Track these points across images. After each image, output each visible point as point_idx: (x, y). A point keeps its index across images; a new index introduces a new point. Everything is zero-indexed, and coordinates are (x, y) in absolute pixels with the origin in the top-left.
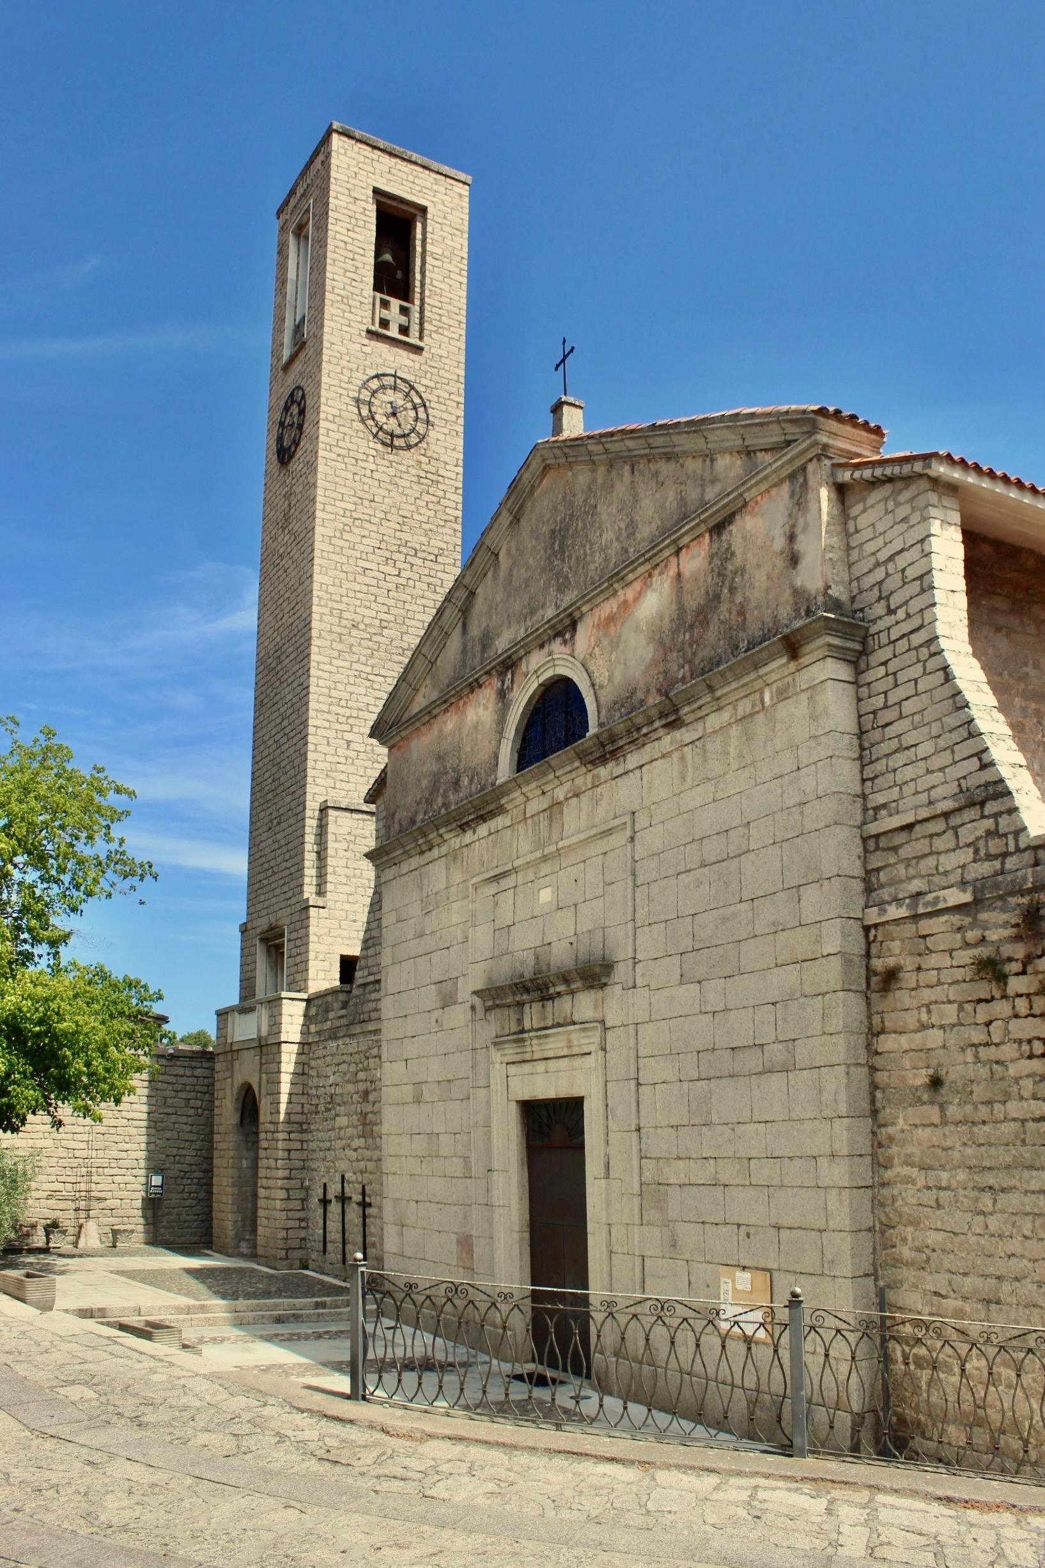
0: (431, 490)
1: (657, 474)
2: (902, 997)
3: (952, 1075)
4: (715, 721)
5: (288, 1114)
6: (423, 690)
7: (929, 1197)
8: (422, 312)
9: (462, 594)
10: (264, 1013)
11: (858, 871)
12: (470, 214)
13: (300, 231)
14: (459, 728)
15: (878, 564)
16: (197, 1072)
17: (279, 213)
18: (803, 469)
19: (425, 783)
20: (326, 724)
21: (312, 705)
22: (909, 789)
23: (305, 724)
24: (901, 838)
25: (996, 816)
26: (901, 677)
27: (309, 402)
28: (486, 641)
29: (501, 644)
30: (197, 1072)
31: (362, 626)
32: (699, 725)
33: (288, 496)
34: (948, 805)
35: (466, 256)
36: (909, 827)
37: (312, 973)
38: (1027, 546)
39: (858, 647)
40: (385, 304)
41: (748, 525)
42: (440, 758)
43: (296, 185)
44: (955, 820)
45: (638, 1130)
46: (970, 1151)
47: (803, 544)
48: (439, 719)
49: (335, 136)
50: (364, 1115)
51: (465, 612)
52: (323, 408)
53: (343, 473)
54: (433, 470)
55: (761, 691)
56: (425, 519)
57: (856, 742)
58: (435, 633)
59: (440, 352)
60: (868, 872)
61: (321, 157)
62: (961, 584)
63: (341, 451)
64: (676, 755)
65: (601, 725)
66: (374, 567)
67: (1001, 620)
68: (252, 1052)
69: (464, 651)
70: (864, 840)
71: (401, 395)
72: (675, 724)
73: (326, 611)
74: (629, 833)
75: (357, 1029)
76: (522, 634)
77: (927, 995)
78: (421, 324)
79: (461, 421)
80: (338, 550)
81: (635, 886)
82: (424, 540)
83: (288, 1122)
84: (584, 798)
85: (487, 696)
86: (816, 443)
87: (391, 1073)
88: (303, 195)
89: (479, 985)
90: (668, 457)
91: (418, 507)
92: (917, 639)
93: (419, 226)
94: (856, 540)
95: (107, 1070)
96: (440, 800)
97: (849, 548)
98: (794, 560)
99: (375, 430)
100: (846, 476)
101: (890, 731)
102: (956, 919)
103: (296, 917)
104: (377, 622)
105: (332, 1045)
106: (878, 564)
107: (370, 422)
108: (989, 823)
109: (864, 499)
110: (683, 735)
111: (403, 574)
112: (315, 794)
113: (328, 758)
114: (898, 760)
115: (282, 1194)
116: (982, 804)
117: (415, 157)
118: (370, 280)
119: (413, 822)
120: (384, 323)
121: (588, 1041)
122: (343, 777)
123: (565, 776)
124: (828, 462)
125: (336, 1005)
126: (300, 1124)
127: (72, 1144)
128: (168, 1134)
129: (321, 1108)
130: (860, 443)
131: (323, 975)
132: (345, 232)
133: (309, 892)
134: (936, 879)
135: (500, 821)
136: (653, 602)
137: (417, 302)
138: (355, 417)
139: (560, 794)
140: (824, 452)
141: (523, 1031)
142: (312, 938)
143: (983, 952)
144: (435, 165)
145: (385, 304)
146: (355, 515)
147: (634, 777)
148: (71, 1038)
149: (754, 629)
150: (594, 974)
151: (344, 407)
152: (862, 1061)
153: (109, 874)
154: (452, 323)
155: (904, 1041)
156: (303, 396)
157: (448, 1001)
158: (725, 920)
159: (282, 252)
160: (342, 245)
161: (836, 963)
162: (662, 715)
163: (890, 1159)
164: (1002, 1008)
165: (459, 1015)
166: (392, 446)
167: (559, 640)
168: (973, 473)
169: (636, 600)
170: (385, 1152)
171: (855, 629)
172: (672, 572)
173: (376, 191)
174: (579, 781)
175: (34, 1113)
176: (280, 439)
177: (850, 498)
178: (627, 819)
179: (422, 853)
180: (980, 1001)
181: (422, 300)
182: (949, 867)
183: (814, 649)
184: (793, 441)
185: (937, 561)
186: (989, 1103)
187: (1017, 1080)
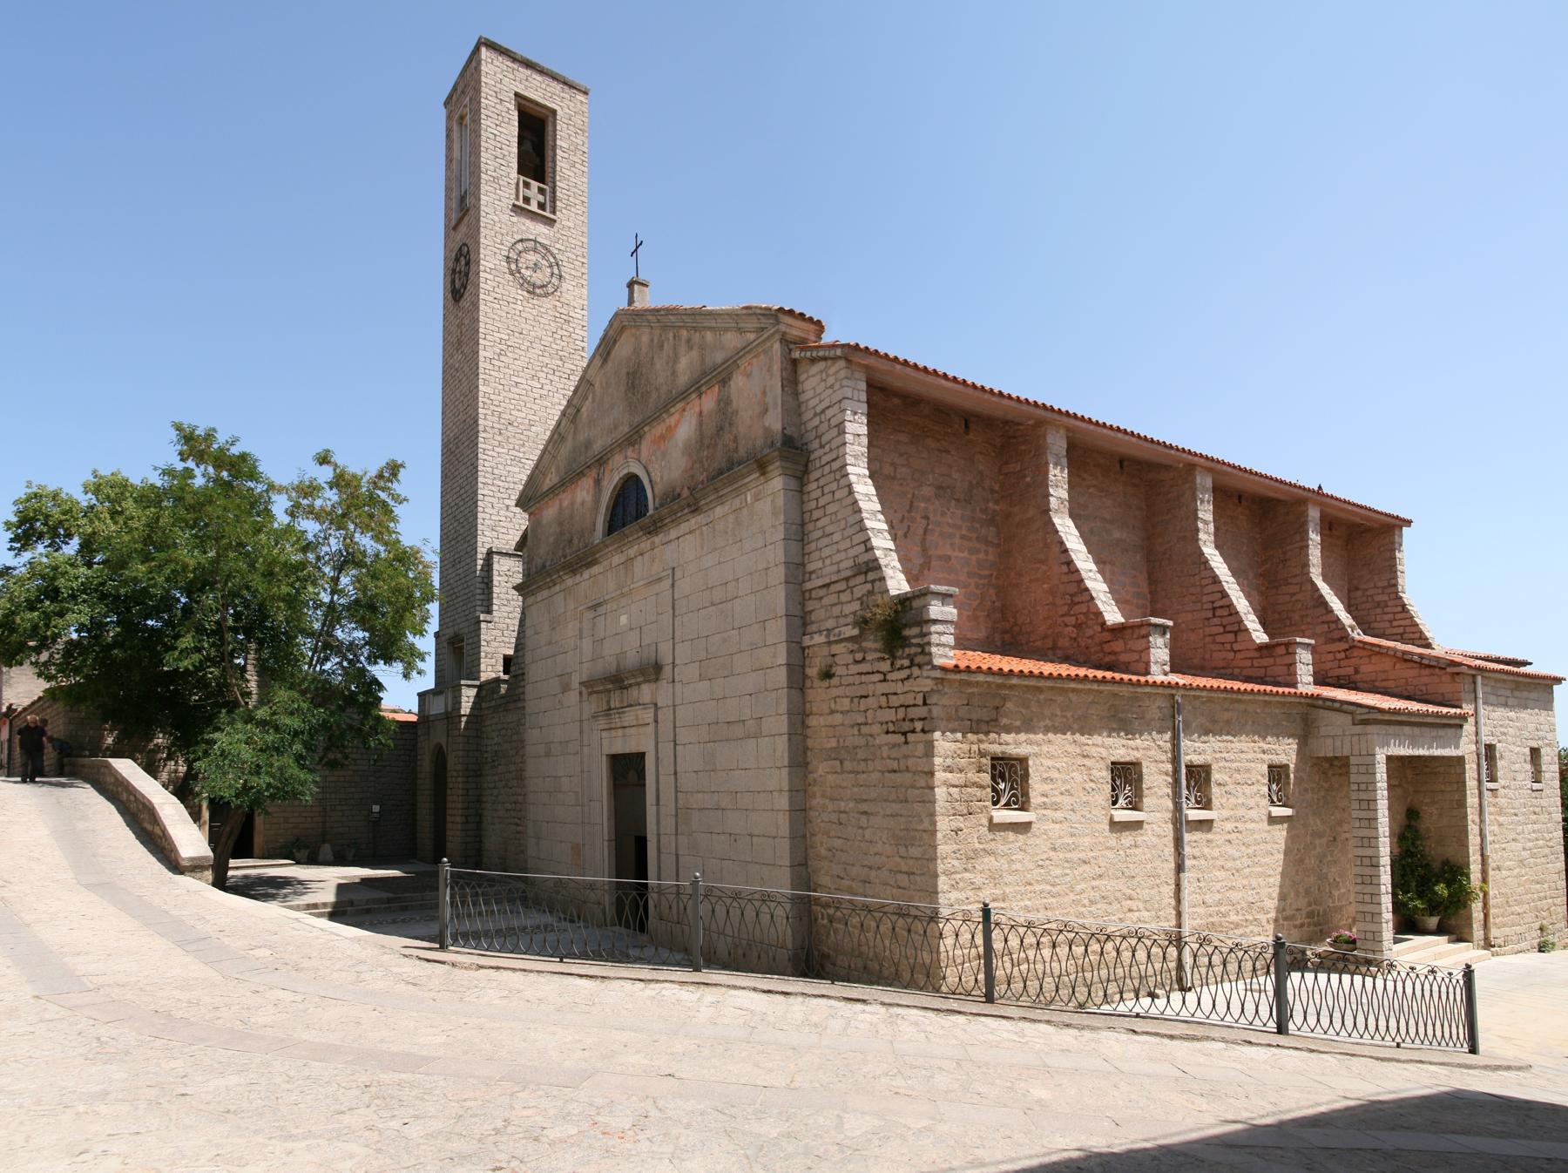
14: (572, 504)
15: (816, 415)
21: (480, 479)
22: (828, 562)
24: (822, 592)
25: (873, 582)
26: (826, 490)
34: (849, 573)
36: (827, 586)
37: (483, 667)
42: (561, 524)
44: (852, 583)
51: (574, 421)
75: (512, 706)
92: (836, 465)
101: (820, 524)
102: (850, 646)
106: (816, 415)
108: (869, 586)
112: (485, 541)
118: (515, 166)
119: (544, 567)
131: (490, 668)
135: (596, 569)
136: (684, 427)
147: (673, 545)
149: (742, 452)
150: (653, 670)
155: (822, 721)
161: (784, 670)
162: (689, 505)
165: (572, 697)
171: (800, 454)
173: (517, 94)
176: (453, 282)
182: (837, 615)
183: (775, 468)
187: (880, 747)
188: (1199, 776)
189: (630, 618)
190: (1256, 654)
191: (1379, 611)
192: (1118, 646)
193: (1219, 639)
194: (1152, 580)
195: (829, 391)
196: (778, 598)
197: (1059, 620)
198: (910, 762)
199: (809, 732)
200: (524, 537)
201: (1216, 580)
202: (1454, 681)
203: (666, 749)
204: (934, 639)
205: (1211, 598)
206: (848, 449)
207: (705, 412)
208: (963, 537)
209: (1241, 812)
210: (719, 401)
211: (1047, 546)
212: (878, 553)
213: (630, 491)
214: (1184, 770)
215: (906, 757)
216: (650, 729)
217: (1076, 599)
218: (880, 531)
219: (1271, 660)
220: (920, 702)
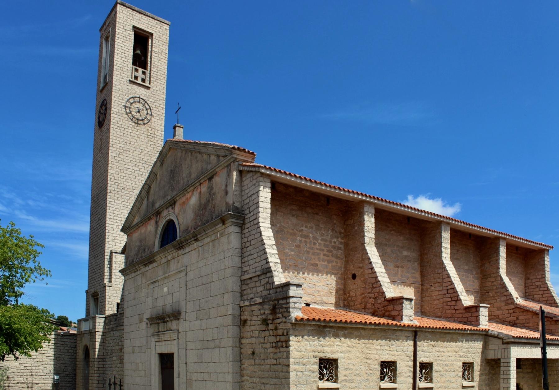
0: (152, 140)
1: (197, 157)
2: (247, 328)
3: (257, 351)
4: (207, 240)
5: (98, 355)
6: (137, 217)
7: (251, 385)
8: (150, 74)
9: (147, 187)
10: (91, 322)
11: (238, 290)
12: (169, 37)
13: (107, 39)
16: (72, 341)
17: (100, 30)
18: (230, 164)
19: (136, 249)
20: (113, 223)
21: (108, 216)
23: (105, 223)
24: (249, 281)
25: (269, 277)
27: (108, 106)
28: (153, 204)
29: (157, 205)
30: (72, 341)
31: (126, 189)
32: (203, 241)
33: (101, 139)
34: (258, 273)
35: (167, 52)
36: (251, 278)
37: (107, 309)
38: (306, 188)
39: (242, 222)
40: (137, 70)
41: (217, 179)
42: (141, 241)
43: (106, 21)
44: (261, 278)
45: (186, 363)
46: (260, 373)
47: (229, 189)
48: (141, 228)
49: (118, 5)
50: (121, 356)
51: (148, 192)
52: (112, 109)
53: (120, 133)
54: (153, 133)
55: (217, 233)
56: (149, 150)
57: (240, 251)
58: (139, 199)
59: (157, 89)
60: (242, 291)
61: (114, 13)
62: (269, 206)
63: (119, 125)
64: (197, 249)
65: (180, 237)
67: (294, 213)
68: (88, 335)
69: (147, 206)
70: (241, 281)
71: (141, 105)
72: (197, 240)
73: (113, 183)
74: (185, 273)
75: (119, 328)
76: (162, 203)
77: (253, 328)
78: (150, 78)
79: (164, 115)
80: (117, 161)
81: (187, 289)
82: (149, 158)
83: (98, 358)
84: (176, 259)
85: (152, 222)
86: (233, 157)
87: (127, 343)
88: (108, 25)
89: (149, 316)
90: (200, 153)
91: (147, 146)
92: (255, 222)
93: (150, 40)
94: (244, 188)
95: (33, 340)
96: (140, 255)
97: (242, 191)
98: (227, 193)
99: (131, 118)
100: (241, 168)
102: (259, 306)
103: (102, 289)
104: (131, 187)
105: (112, 333)
106: (248, 197)
107: (130, 115)
108: (267, 280)
109: (246, 176)
110: (199, 244)
111: (141, 170)
113: (113, 235)
115: (97, 382)
116: (266, 274)
117: (149, 14)
118: (131, 61)
119: (133, 261)
120: (136, 78)
121: (174, 336)
122: (119, 241)
123: (171, 253)
124: (237, 163)
125: (113, 320)
126: (102, 358)
127: (26, 365)
128: (62, 362)
129: (109, 354)
130: (248, 157)
132: (121, 42)
133: (106, 281)
134: (256, 294)
135: (155, 264)
136: (194, 200)
137: (149, 70)
138: (124, 113)
139: (170, 258)
140: (236, 160)
141: (159, 332)
142: (107, 297)
143: (264, 317)
144: (157, 17)
145: (137, 70)
146: (124, 149)
147: (187, 255)
148: (19, 331)
151: (120, 109)
152: (238, 346)
153: (35, 273)
154: (161, 78)
156: (106, 103)
157: (141, 321)
158: (207, 302)
159: (101, 46)
160: (120, 47)
161: (231, 317)
162: (193, 237)
163: (244, 374)
164: (267, 333)
165: (143, 325)
166: (138, 123)
167: (171, 208)
168: (274, 171)
169: (190, 198)
170: (125, 368)
171: (243, 217)
172: (199, 191)
173: (134, 27)
174: (174, 254)
175: (8, 355)
176: (99, 118)
177: (243, 175)
178: (185, 268)
179: (135, 272)
180: (263, 331)
181: (150, 69)
182: (257, 292)
183: (229, 222)
184: (228, 155)
185: (261, 199)
186: (264, 359)
187: (270, 353)
188: (426, 368)
189: (168, 289)
190: (464, 312)
191: (537, 289)
192: (390, 307)
193: (449, 304)
194: (422, 275)
195: (254, 187)
197: (367, 295)
198: (281, 360)
200: (125, 246)
201: (448, 276)
202: (556, 324)
204: (292, 305)
205: (446, 285)
206: (260, 214)
207: (202, 192)
208: (324, 255)
209: (447, 384)
210: (208, 188)
211: (363, 260)
212: (271, 265)
213: (170, 227)
214: (418, 365)
215: (280, 358)
217: (374, 286)
218: (273, 254)
219: (470, 314)
220: (285, 334)
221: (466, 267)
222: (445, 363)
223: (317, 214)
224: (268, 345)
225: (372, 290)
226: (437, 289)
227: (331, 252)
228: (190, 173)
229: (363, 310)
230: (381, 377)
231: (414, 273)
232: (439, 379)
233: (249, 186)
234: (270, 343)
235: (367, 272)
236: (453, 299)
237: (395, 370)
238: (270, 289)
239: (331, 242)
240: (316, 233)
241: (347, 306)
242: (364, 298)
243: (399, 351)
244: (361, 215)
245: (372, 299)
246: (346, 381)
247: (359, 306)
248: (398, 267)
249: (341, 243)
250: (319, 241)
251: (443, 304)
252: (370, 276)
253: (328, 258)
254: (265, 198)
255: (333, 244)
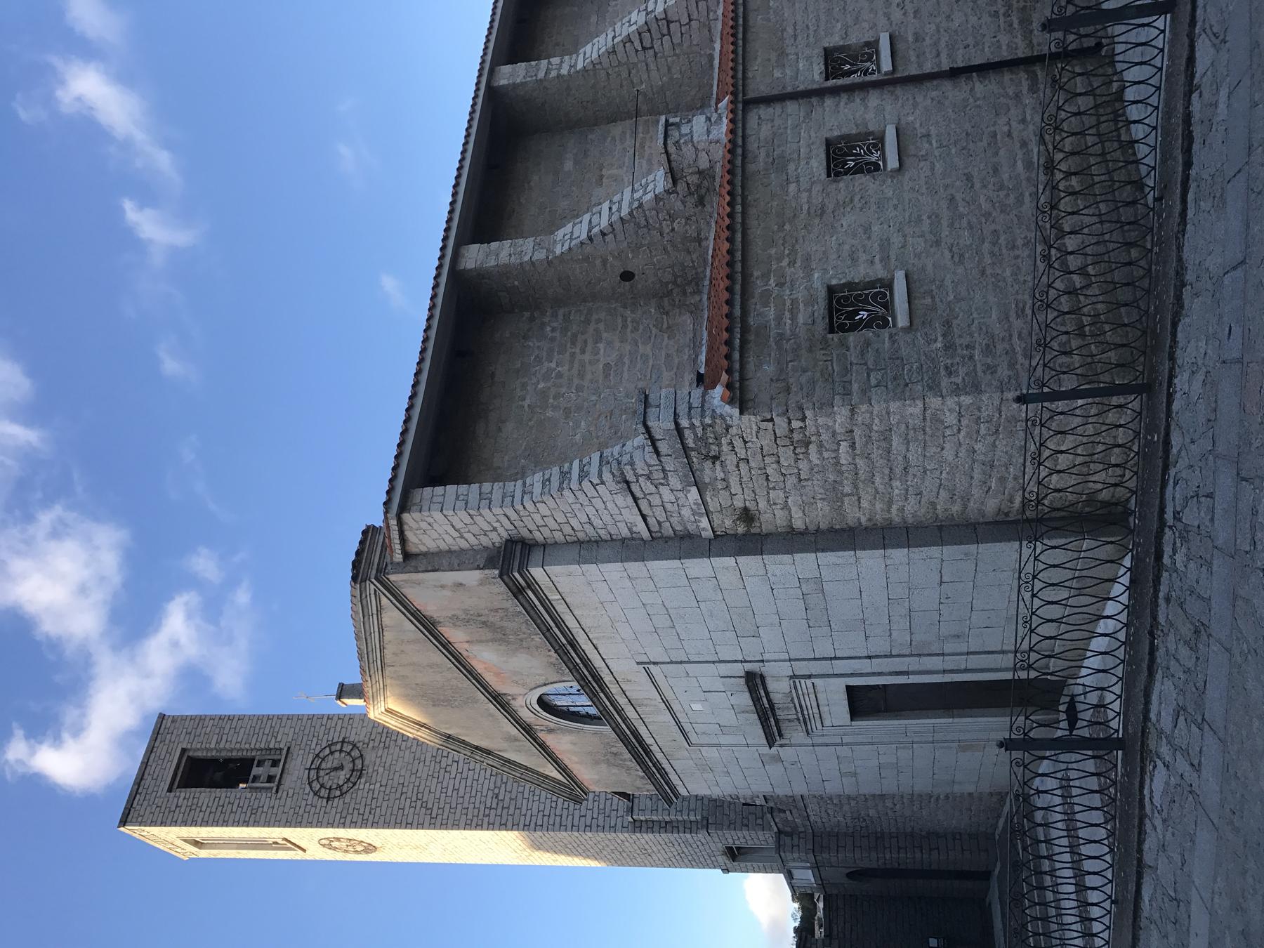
7: (912, 500)
15: (462, 537)
19: (615, 771)
22: (619, 518)
24: (651, 521)
31: (496, 791)
36: (644, 517)
39: (519, 547)
42: (597, 763)
44: (639, 494)
46: (878, 480)
66: (452, 781)
73: (486, 819)
101: (577, 526)
106: (462, 537)
107: (345, 788)
114: (597, 522)
125: (782, 815)
146: (414, 799)
150: (754, 682)
157: (778, 759)
165: (786, 753)
172: (466, 646)
193: (677, 40)
194: (613, 119)
195: (435, 526)
196: (663, 568)
199: (812, 528)
203: (840, 667)
207: (468, 638)
208: (583, 352)
214: (831, 83)
216: (817, 681)
217: (643, 222)
221: (594, 19)
222: (823, 18)
223: (493, 375)
224: (803, 465)
225: (655, 228)
226: (645, 77)
227: (575, 336)
228: (430, 666)
229: (704, 243)
230: (869, 171)
231: (614, 139)
232: (865, 25)
233: (435, 535)
234: (797, 460)
235: (612, 246)
236: (665, 31)
237: (846, 138)
238: (664, 470)
239: (553, 339)
240: (534, 374)
241: (697, 285)
242: (674, 246)
243: (798, 138)
244: (481, 275)
245: (675, 225)
246: (885, 259)
247: (694, 256)
248: (601, 177)
249: (555, 315)
250: (553, 365)
251: (678, 56)
252: (620, 237)
253: (590, 342)
254: (457, 498)
255: (557, 334)
